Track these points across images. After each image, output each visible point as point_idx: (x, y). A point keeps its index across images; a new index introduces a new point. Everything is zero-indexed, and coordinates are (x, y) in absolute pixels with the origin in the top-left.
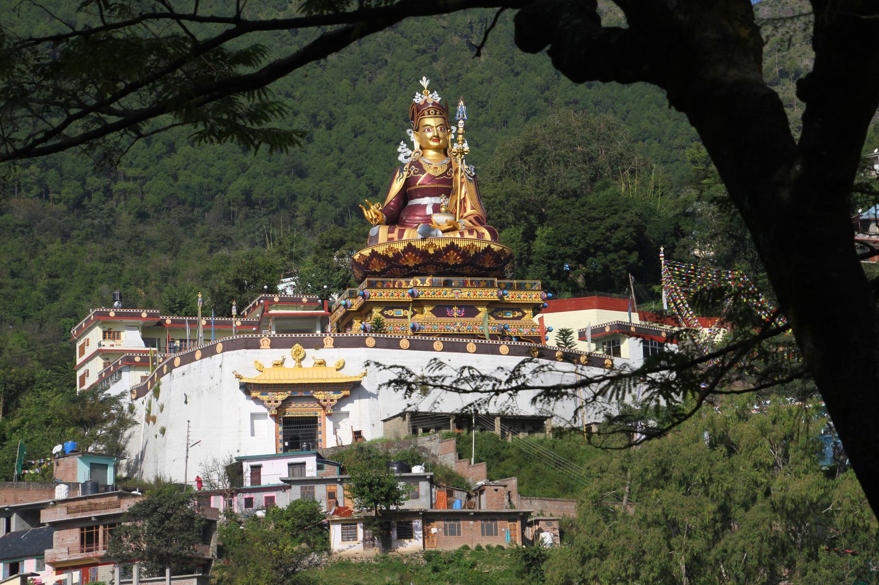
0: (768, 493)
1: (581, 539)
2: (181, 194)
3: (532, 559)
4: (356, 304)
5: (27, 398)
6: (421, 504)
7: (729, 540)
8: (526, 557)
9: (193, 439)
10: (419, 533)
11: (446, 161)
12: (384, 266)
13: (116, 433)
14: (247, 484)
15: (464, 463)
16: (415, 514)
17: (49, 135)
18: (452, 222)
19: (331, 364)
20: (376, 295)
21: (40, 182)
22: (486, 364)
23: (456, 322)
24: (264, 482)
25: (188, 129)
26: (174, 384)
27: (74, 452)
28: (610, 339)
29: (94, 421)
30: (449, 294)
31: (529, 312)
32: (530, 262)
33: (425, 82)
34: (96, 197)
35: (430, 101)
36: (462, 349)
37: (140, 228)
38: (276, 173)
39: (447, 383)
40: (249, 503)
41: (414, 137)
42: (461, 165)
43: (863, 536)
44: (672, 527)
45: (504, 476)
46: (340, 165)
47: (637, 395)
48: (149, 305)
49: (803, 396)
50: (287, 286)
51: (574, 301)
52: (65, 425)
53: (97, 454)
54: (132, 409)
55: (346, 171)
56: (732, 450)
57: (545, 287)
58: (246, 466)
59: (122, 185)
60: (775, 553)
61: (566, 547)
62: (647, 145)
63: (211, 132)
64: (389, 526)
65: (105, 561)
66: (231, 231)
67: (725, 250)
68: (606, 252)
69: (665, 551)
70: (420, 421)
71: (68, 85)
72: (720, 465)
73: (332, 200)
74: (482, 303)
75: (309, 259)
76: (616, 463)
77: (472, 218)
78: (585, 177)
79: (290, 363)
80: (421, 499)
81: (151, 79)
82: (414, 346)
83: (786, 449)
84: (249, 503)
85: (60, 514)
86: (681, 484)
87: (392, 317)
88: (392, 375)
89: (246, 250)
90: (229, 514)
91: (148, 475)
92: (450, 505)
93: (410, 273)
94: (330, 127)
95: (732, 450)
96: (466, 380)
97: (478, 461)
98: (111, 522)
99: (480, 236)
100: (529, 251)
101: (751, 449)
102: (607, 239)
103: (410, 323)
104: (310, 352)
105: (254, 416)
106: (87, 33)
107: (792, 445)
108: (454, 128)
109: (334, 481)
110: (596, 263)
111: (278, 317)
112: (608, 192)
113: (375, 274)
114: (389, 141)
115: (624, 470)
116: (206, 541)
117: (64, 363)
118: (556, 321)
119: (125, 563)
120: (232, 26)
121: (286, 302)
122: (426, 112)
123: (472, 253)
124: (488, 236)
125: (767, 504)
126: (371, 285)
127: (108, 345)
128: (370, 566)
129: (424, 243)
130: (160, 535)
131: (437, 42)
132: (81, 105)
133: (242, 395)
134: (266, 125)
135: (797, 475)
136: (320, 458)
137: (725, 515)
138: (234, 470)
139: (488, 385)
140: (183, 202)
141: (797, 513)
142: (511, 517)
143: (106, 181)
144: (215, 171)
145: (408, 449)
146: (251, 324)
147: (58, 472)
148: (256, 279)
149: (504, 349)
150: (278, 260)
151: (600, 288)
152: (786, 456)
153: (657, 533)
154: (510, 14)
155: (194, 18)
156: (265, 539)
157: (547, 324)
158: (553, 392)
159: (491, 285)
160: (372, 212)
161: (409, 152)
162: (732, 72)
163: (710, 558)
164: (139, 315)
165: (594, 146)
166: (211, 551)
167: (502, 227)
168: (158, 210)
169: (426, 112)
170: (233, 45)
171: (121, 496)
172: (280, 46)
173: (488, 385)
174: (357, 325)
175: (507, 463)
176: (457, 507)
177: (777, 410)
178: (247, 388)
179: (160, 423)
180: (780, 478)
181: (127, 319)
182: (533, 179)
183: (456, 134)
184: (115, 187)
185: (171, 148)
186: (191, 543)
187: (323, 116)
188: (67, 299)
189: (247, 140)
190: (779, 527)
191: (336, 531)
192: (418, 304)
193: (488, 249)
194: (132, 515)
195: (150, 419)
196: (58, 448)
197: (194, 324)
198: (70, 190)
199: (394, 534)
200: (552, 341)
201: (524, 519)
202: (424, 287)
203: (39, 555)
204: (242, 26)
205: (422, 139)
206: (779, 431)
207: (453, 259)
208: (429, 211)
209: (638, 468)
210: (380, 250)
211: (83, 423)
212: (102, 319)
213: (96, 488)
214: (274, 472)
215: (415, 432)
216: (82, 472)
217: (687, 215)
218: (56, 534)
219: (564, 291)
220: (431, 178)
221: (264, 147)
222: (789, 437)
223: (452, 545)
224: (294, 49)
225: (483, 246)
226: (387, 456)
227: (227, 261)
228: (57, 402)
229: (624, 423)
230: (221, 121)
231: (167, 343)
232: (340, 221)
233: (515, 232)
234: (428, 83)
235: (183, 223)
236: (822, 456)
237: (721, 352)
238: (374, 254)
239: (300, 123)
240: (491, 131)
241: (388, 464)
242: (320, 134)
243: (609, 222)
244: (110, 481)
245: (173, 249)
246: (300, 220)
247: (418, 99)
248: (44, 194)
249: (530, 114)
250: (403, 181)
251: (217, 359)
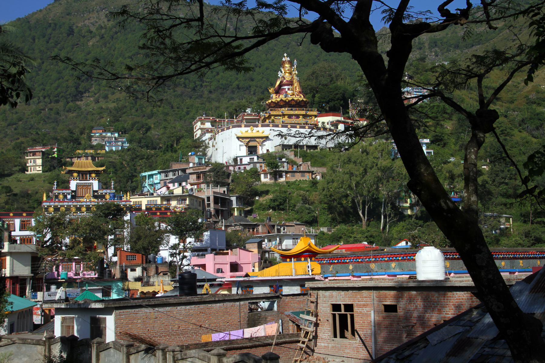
0: (377, 165)
1: (327, 178)
2: (221, 86)
3: (314, 183)
4: (267, 115)
5: (182, 141)
6: (285, 169)
7: (366, 178)
8: (313, 183)
9: (225, 151)
10: (284, 176)
13: (204, 150)
14: (239, 163)
15: (296, 158)
16: (283, 171)
17: (187, 69)
18: (293, 93)
19: (261, 131)
20: (272, 113)
21: (184, 83)
22: (302, 131)
23: (294, 120)
24: (243, 163)
25: (223, 67)
26: (219, 137)
27: (194, 155)
28: (335, 124)
29: (199, 146)
30: (292, 112)
31: (314, 117)
32: (314, 104)
33: (285, 55)
34: (198, 87)
36: (296, 127)
37: (210, 95)
38: (245, 80)
39: (292, 135)
40: (239, 168)
41: (282, 70)
42: (295, 77)
43: (401, 176)
44: (352, 174)
45: (307, 161)
46: (263, 78)
47: (343, 138)
48: (212, 116)
49: (387, 139)
50: (249, 111)
51: (326, 114)
52: (191, 148)
53: (200, 155)
54: (208, 143)
55: (264, 79)
56: (367, 154)
57: (318, 111)
58: (238, 159)
59: (205, 84)
60: (378, 181)
61: (323, 180)
62: (347, 70)
63: (229, 68)
64: (276, 175)
65: (203, 183)
66: (234, 96)
67: (367, 100)
68: (334, 101)
69: (349, 180)
70: (285, 147)
71: (191, 56)
72: (364, 158)
73: (261, 87)
74: (301, 115)
75: (254, 103)
76: (337, 157)
78: (329, 80)
79: (250, 131)
80: (286, 167)
81: (213, 53)
82: (283, 127)
83: (382, 153)
84: (239, 168)
85: (191, 171)
86: (354, 163)
88: (277, 133)
89: (238, 101)
90: (234, 171)
91: (213, 161)
92: (292, 169)
94: (260, 67)
95: (367, 154)
96: (297, 134)
97: (300, 157)
98: (204, 173)
99: (300, 97)
100: (314, 101)
101: (372, 154)
102: (335, 97)
103: (281, 120)
104: (255, 128)
105: (240, 145)
106: (197, 41)
107: (384, 152)
109: (262, 163)
110: (332, 104)
111: (246, 119)
112: (335, 84)
113: (272, 107)
114: (276, 71)
115: (339, 159)
116: (229, 178)
117: (191, 131)
118: (321, 120)
119: (208, 184)
120: (234, 39)
121: (248, 115)
124: (302, 97)
125: (376, 168)
126: (271, 110)
127: (202, 126)
128: (272, 185)
130: (216, 177)
131: (289, 44)
132: (195, 61)
133: (237, 140)
134: (243, 66)
135: (385, 160)
136: (258, 157)
137: (365, 171)
138: (235, 160)
139: (303, 135)
140: (221, 88)
141: (384, 170)
142: (309, 172)
143: (201, 83)
144: (229, 80)
145: (281, 154)
146: (239, 121)
147: (190, 160)
148: (240, 109)
149: (307, 127)
150: (247, 103)
151: (333, 111)
152: (382, 155)
153: (348, 176)
154: (309, 34)
155: (224, 36)
156: (244, 178)
157: (318, 121)
158: (320, 137)
159: (303, 110)
160: (271, 90)
162: (369, 49)
163: (361, 182)
164: (210, 119)
165: (331, 72)
166: (230, 181)
167: (306, 94)
168: (214, 90)
170: (234, 44)
171: (206, 166)
172: (247, 44)
173: (303, 135)
174: (267, 121)
175: (307, 158)
176: (294, 170)
177: (380, 143)
178: (238, 138)
179: (216, 147)
180: (380, 161)
181: (207, 120)
182: (314, 81)
184: (204, 84)
185: (218, 74)
186: (224, 179)
187: (258, 64)
188: (191, 114)
189: (239, 70)
190: (379, 174)
191: (262, 176)
192: (284, 115)
194: (209, 171)
195: (213, 146)
196: (190, 154)
197: (224, 121)
198: (192, 85)
199: (278, 177)
200: (320, 125)
201: (312, 173)
202: (286, 111)
203: (186, 181)
204: (237, 39)
205: (285, 70)
206: (380, 148)
207: (293, 103)
208: (287, 90)
209: (343, 159)
210: (274, 100)
211: (196, 147)
212: (200, 120)
213: (200, 164)
214: (246, 160)
215: (283, 150)
216: (196, 160)
217: (356, 91)
218: (190, 176)
219: (323, 112)
220: (287, 81)
221: (243, 72)
222: (383, 150)
223: (293, 180)
224: (252, 44)
225: (301, 99)
226: (276, 156)
227: (233, 104)
228: (189, 142)
229: (339, 146)
230: (231, 65)
231: (217, 126)
232: (263, 93)
233: (310, 95)
235: (221, 94)
236: (391, 155)
237: (366, 126)
238: (272, 102)
239: (252, 66)
240: (303, 68)
241: (276, 158)
242: (257, 69)
243: (335, 93)
244: (203, 162)
245: (219, 101)
246: (252, 93)
247: (284, 59)
248: (185, 87)
249: (314, 63)
251: (230, 130)
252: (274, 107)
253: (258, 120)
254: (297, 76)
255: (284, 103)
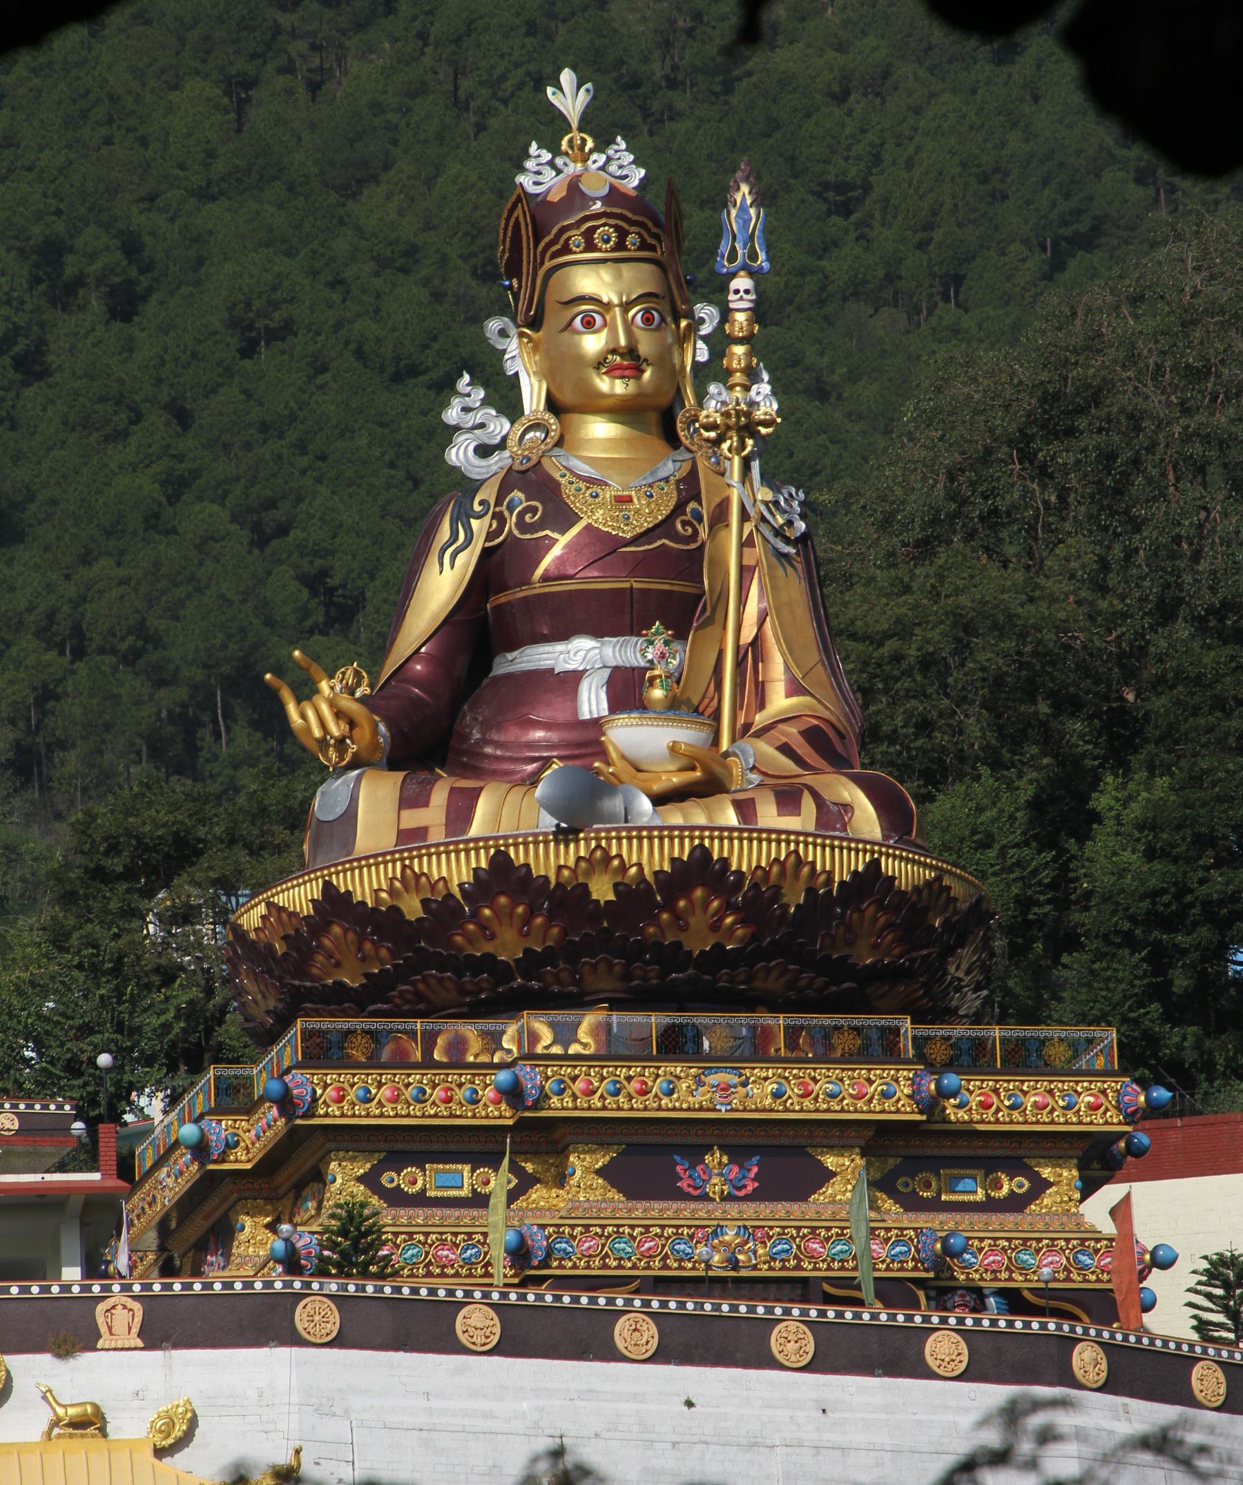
4: (248, 1139)
11: (670, 467)
12: (382, 959)
18: (696, 749)
20: (346, 1096)
23: (722, 1224)
30: (683, 1091)
33: (569, 96)
35: (595, 187)
41: (519, 359)
42: (739, 487)
46: (176, 486)
57: (1137, 1059)
73: (140, 648)
74: (839, 1133)
77: (792, 730)
87: (420, 1200)
93: (501, 993)
94: (124, 305)
99: (833, 818)
108: (707, 313)
113: (336, 999)
114: (403, 373)
122: (576, 238)
123: (795, 898)
124: (866, 818)
126: (321, 1053)
129: (570, 854)
149: (944, 1348)
159: (884, 1049)
160: (321, 711)
161: (499, 426)
167: (935, 776)
169: (576, 238)
174: (255, 1238)
182: (1078, 549)
183: (719, 342)
192: (538, 1140)
193: (871, 881)
202: (570, 1055)
207: (704, 926)
208: (592, 701)
210: (364, 886)
220: (603, 547)
225: (842, 865)
232: (175, 748)
233: (994, 800)
234: (583, 97)
238: (335, 903)
247: (540, 175)
249: (1062, 248)
250: (467, 560)
252: (372, 996)
253: (97, 1221)
254: (778, 459)
255: (545, 934)
